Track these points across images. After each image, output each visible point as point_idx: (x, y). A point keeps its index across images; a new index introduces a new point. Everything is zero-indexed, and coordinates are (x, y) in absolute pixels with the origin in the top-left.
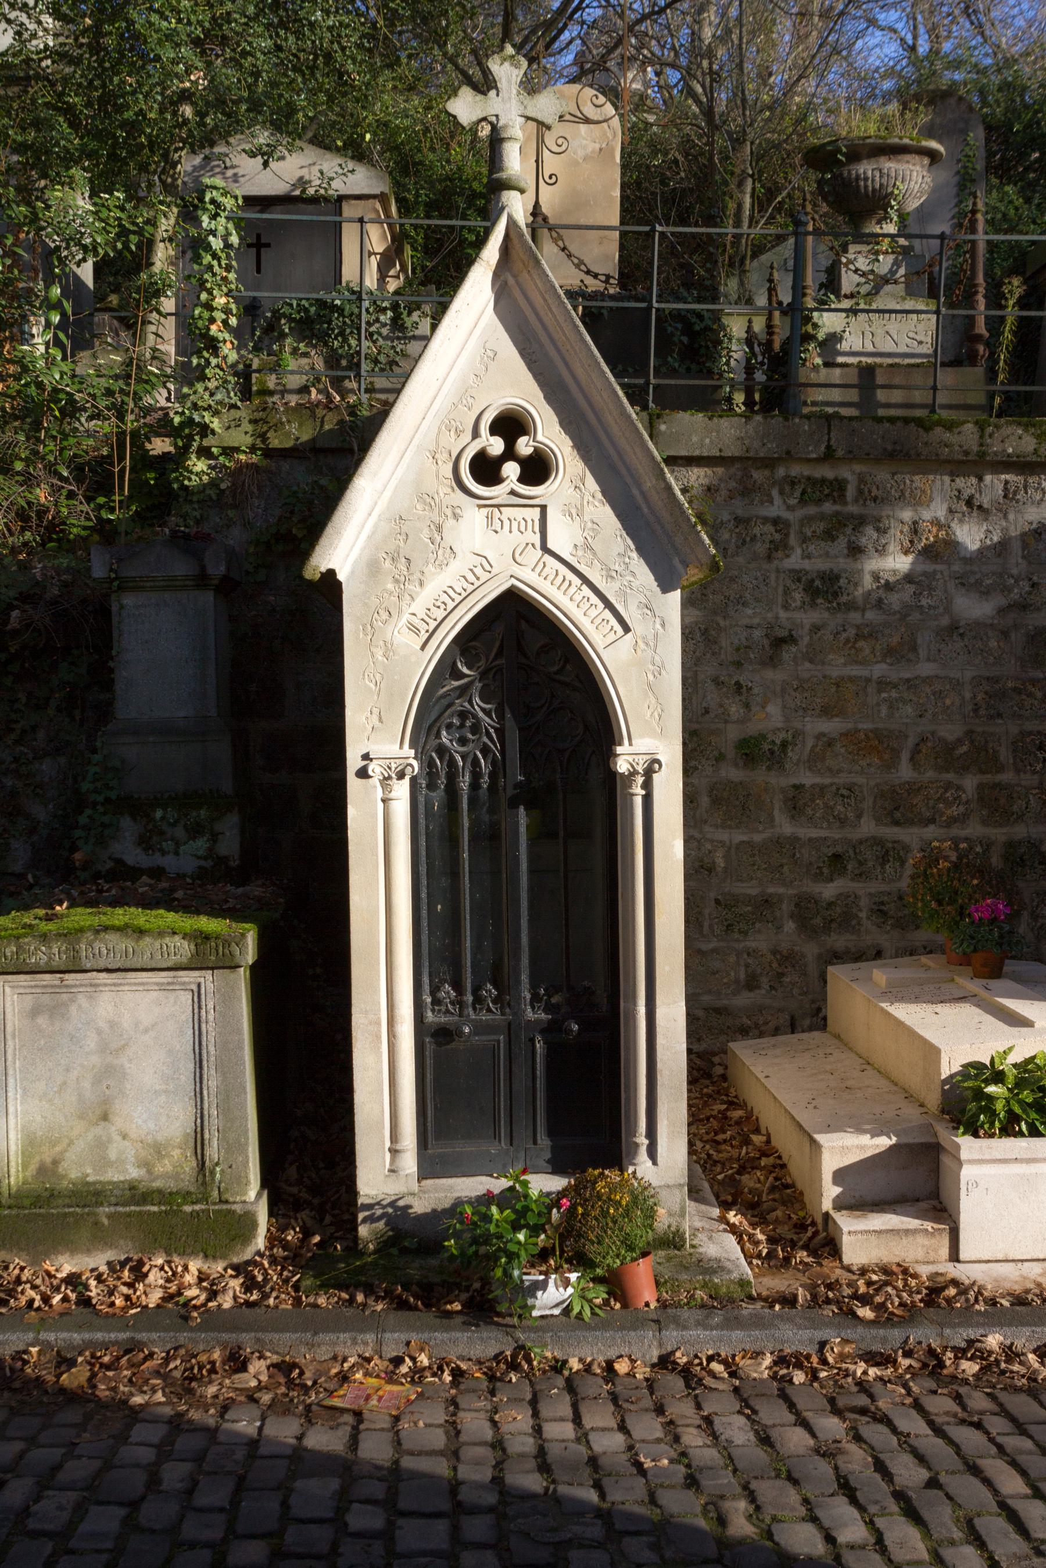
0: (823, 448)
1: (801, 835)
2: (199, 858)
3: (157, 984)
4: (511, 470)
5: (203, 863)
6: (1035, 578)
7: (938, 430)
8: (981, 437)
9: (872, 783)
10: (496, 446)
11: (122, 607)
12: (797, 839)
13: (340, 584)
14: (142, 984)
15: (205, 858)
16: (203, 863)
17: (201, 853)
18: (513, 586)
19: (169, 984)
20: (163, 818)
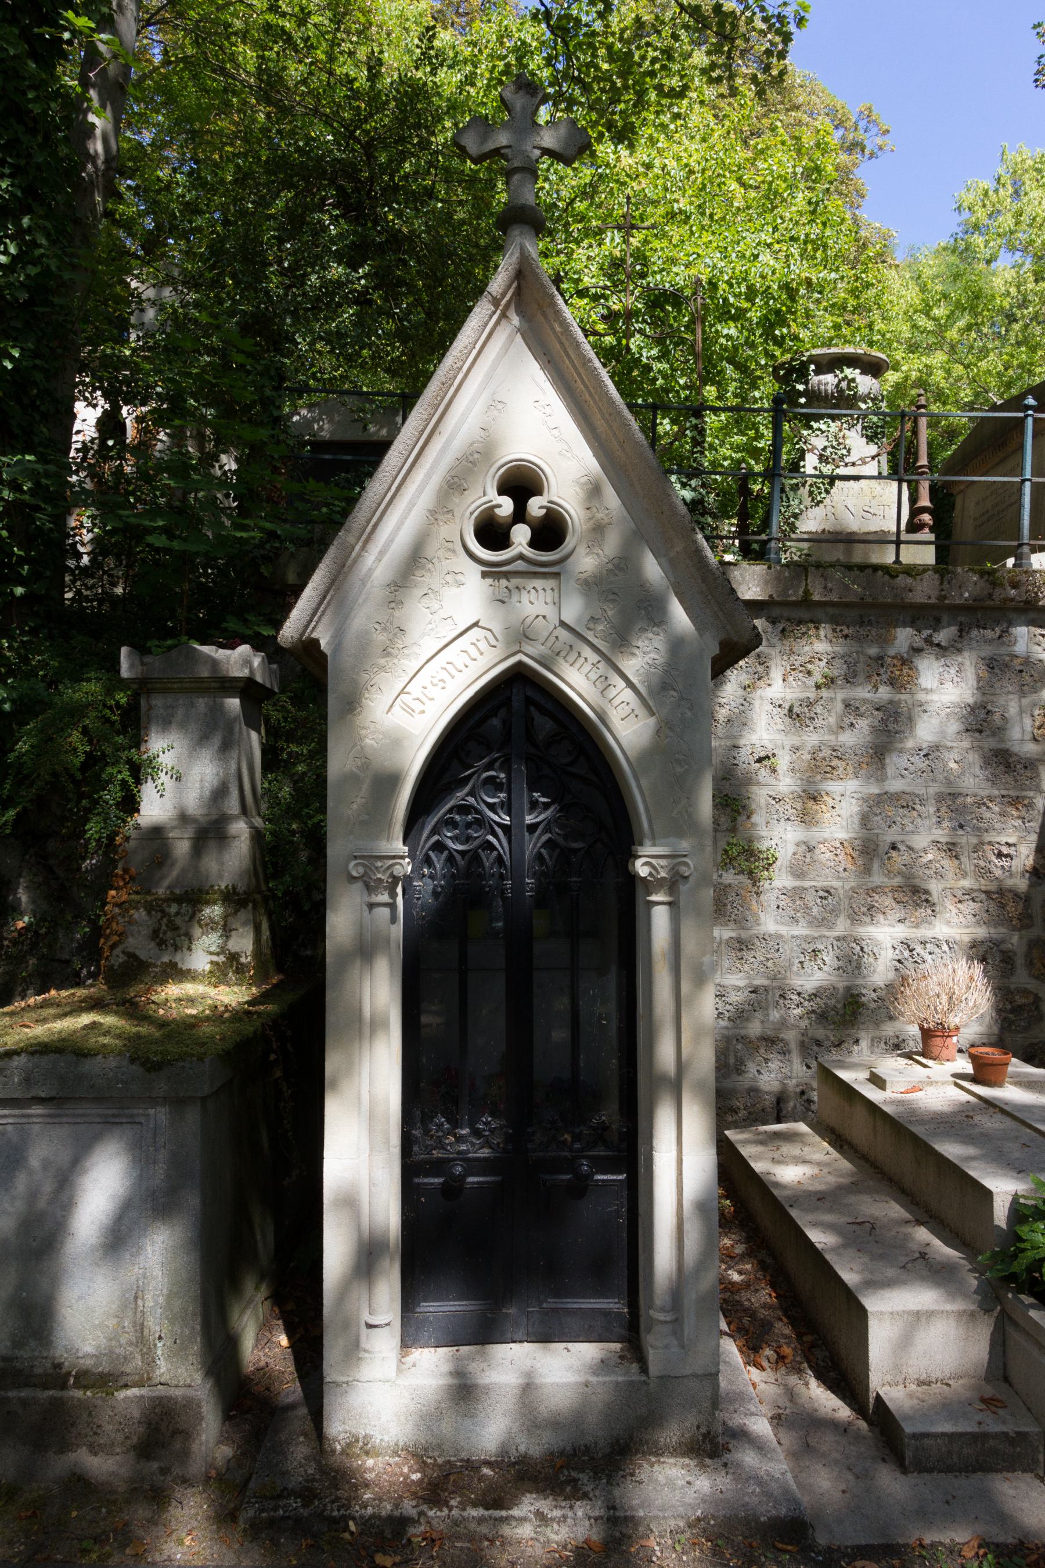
0: (801, 592)
1: (784, 933)
2: (211, 953)
3: (100, 1116)
4: (521, 534)
5: (215, 958)
6: (989, 707)
7: (901, 576)
8: (941, 584)
9: (847, 887)
10: (506, 506)
11: (150, 708)
12: (781, 936)
13: (324, 656)
14: (83, 1115)
15: (218, 954)
16: (215, 958)
17: (213, 949)
18: (520, 663)
19: (114, 1116)
20: (178, 914)
